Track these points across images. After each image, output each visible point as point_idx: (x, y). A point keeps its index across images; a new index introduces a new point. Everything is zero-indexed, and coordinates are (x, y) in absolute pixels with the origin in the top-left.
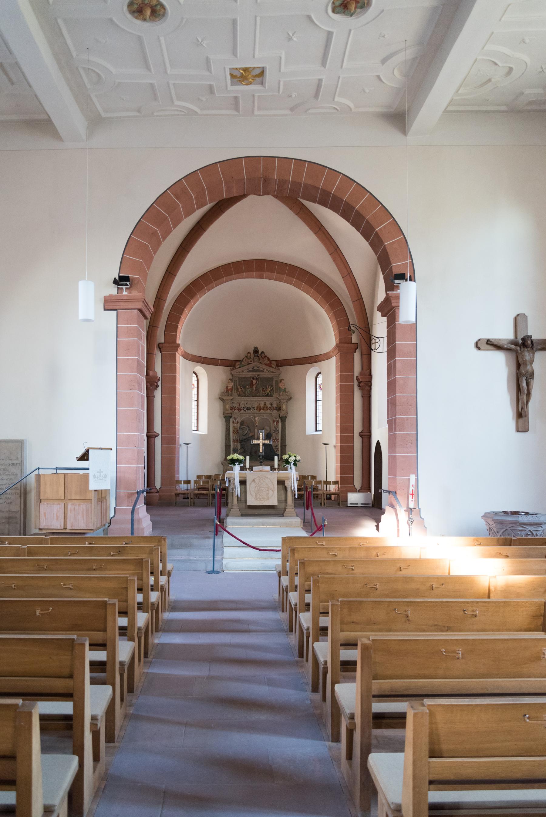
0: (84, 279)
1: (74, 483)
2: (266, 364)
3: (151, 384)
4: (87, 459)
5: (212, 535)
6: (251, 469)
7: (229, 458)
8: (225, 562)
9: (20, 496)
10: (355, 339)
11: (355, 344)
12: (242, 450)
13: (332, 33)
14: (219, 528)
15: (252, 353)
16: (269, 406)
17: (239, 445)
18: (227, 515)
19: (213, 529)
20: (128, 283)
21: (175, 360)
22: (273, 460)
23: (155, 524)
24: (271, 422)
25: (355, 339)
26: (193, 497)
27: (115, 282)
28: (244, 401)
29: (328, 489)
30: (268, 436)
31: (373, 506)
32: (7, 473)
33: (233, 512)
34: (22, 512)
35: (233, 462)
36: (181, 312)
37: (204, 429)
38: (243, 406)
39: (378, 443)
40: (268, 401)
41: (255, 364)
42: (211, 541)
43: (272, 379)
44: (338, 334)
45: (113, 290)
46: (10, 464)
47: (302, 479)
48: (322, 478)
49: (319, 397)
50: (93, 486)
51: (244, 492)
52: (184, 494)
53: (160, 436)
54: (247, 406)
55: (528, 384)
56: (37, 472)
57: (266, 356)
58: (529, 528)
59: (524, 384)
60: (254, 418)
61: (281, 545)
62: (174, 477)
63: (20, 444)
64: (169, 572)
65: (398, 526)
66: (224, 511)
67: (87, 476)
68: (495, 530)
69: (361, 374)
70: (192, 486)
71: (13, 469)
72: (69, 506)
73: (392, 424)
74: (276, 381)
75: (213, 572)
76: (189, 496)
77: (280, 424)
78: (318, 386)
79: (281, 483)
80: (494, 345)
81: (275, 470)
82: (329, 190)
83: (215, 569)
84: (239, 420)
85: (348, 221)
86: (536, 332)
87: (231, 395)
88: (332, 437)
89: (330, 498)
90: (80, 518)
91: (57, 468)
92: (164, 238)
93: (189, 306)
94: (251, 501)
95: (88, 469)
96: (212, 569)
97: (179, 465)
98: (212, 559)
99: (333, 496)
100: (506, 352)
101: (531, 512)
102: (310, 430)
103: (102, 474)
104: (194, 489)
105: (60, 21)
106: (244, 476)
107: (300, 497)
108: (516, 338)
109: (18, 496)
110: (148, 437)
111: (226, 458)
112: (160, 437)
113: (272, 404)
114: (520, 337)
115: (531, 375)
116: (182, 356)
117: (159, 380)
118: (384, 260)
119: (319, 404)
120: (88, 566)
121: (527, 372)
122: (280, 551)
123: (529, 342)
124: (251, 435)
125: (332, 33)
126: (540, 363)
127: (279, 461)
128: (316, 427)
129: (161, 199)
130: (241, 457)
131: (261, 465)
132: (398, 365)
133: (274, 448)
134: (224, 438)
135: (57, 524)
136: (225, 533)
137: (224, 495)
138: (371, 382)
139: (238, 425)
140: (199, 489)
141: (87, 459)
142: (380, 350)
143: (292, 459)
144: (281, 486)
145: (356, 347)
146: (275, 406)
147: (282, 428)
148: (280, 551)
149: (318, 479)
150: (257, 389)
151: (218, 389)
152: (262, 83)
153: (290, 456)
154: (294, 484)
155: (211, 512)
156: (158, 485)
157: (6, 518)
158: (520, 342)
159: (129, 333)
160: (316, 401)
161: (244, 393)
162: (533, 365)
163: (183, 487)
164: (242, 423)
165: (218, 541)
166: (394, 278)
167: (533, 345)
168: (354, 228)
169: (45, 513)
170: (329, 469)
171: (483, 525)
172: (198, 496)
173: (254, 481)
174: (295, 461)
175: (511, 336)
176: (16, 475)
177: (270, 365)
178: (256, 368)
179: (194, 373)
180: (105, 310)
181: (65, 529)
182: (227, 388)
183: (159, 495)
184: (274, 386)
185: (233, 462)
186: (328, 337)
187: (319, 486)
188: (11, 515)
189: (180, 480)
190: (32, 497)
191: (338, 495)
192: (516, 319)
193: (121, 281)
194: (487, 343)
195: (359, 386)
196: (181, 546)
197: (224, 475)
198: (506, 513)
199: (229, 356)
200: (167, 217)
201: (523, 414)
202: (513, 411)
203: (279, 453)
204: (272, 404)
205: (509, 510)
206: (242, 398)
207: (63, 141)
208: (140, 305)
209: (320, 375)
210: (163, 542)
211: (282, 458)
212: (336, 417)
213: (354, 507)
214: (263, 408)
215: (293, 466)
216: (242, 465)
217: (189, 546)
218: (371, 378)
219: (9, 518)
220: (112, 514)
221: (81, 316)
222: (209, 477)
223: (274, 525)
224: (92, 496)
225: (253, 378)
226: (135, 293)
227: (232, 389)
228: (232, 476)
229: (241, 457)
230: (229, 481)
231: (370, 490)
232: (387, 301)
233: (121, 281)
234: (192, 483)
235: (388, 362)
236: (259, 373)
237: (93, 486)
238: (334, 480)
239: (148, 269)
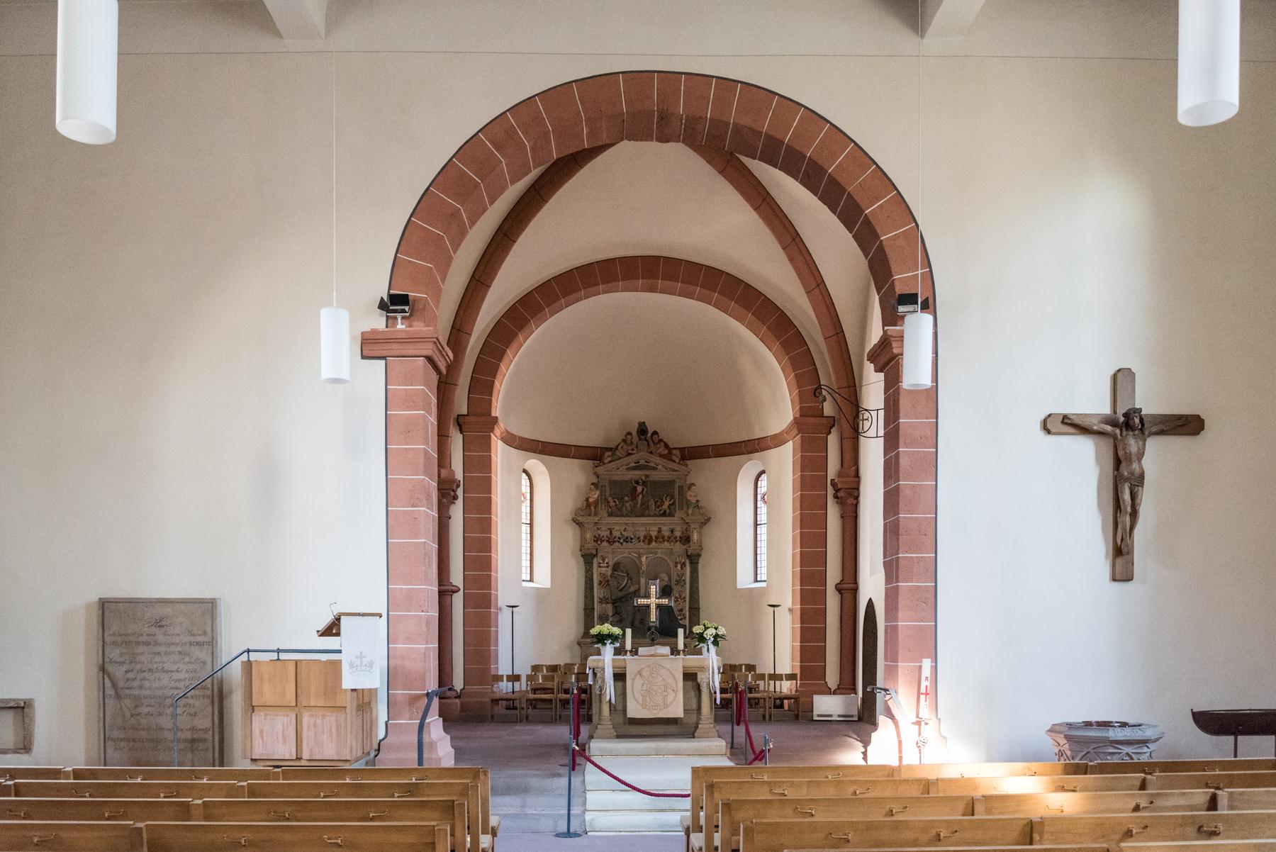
0: (329, 304)
1: (315, 680)
2: (660, 456)
3: (446, 492)
4: (338, 634)
5: (565, 770)
6: (634, 652)
7: (594, 631)
8: (588, 817)
9: (213, 702)
10: (828, 409)
11: (829, 419)
14: (577, 758)
15: (634, 432)
16: (666, 534)
17: (609, 609)
18: (591, 737)
19: (567, 760)
20: (407, 308)
21: (489, 449)
22: (676, 636)
23: (459, 753)
24: (672, 566)
25: (828, 409)
26: (524, 705)
27: (382, 306)
28: (619, 525)
29: (778, 689)
30: (665, 592)
31: (860, 719)
32: (187, 659)
34: (217, 731)
35: (601, 638)
36: (500, 355)
37: (543, 578)
38: (616, 534)
39: (870, 604)
40: (666, 525)
41: (641, 456)
42: (563, 782)
43: (672, 482)
44: (797, 400)
45: (378, 322)
46: (191, 644)
47: (729, 670)
49: (763, 518)
50: (348, 682)
51: (622, 694)
52: (507, 700)
53: (461, 592)
55: (1133, 496)
56: (244, 657)
57: (661, 440)
58: (1126, 749)
59: (1126, 496)
60: (640, 557)
61: (689, 787)
63: (209, 607)
64: (493, 829)
65: (900, 751)
66: (584, 730)
68: (1069, 753)
69: (840, 474)
70: (522, 685)
71: (198, 653)
72: (306, 719)
73: (892, 570)
75: (568, 834)
76: (517, 703)
79: (690, 677)
80: (1074, 425)
81: (678, 653)
82: (780, 137)
83: (572, 830)
84: (611, 560)
85: (816, 194)
86: (1149, 401)
87: (596, 515)
88: (786, 593)
89: (781, 706)
90: (327, 741)
91: (279, 651)
92: (473, 223)
93: (514, 345)
94: (635, 709)
95: (340, 651)
96: (565, 830)
97: (497, 645)
99: (786, 702)
100: (1095, 437)
101: (1131, 722)
102: (744, 579)
103: (364, 662)
104: (527, 691)
107: (726, 704)
108: (1115, 412)
109: (207, 701)
110: (442, 593)
111: (586, 634)
112: (463, 592)
113: (672, 531)
114: (1121, 411)
115: (1139, 480)
116: (502, 439)
117: (458, 486)
118: (880, 268)
119: (762, 530)
120: (359, 810)
121: (1132, 473)
122: (688, 796)
123: (1137, 421)
124: (632, 589)
126: (1156, 457)
127: (685, 637)
129: (467, 150)
131: (652, 645)
132: (904, 462)
133: (677, 613)
134: (582, 595)
135: (285, 751)
136: (589, 765)
137: (583, 701)
138: (858, 489)
139: (609, 571)
140: (535, 691)
141: (338, 634)
142: (872, 433)
143: (709, 633)
144: (690, 683)
145: (832, 423)
146: (678, 534)
147: (692, 577)
148: (688, 796)
150: (644, 498)
151: (570, 504)
153: (706, 628)
155: (562, 732)
156: (458, 683)
157: (185, 741)
158: (1122, 419)
160: (756, 525)
161: (620, 510)
162: (1143, 462)
163: (505, 687)
164: (616, 567)
166: (898, 302)
167: (1143, 425)
168: (825, 207)
169: (261, 732)
170: (780, 652)
171: (1049, 745)
172: (533, 703)
173: (640, 673)
174: (716, 636)
175: (1106, 410)
176: (204, 663)
177: (668, 456)
178: (642, 462)
179: (525, 471)
180: (363, 357)
181: (298, 759)
182: (587, 500)
183: (462, 704)
184: (677, 496)
185: (601, 638)
186: (778, 406)
187: (761, 683)
188: (195, 736)
189: (500, 673)
190: (236, 703)
191: (796, 699)
192: (1115, 377)
193: (393, 304)
194: (1063, 422)
195: (836, 497)
196: (508, 791)
197: (583, 665)
198: (1088, 724)
199: (590, 437)
201: (1124, 550)
202: (1107, 545)
203: (687, 622)
204: (672, 531)
205: (1094, 719)
206: (616, 520)
207: (276, 33)
208: (428, 349)
209: (764, 477)
210: (482, 776)
211: (691, 632)
212: (794, 555)
213: (826, 722)
215: (711, 646)
216: (618, 645)
217: (525, 790)
218: (858, 483)
219: (193, 740)
220: (381, 734)
221: (326, 373)
222: (554, 668)
223: (677, 753)
224: (348, 701)
225: (637, 482)
226: (419, 327)
228: (600, 665)
230: (595, 674)
231: (854, 691)
232: (885, 342)
233: (395, 303)
234: (524, 679)
235: (886, 453)
236: (647, 472)
237: (348, 682)
238: (789, 672)
239: (443, 280)
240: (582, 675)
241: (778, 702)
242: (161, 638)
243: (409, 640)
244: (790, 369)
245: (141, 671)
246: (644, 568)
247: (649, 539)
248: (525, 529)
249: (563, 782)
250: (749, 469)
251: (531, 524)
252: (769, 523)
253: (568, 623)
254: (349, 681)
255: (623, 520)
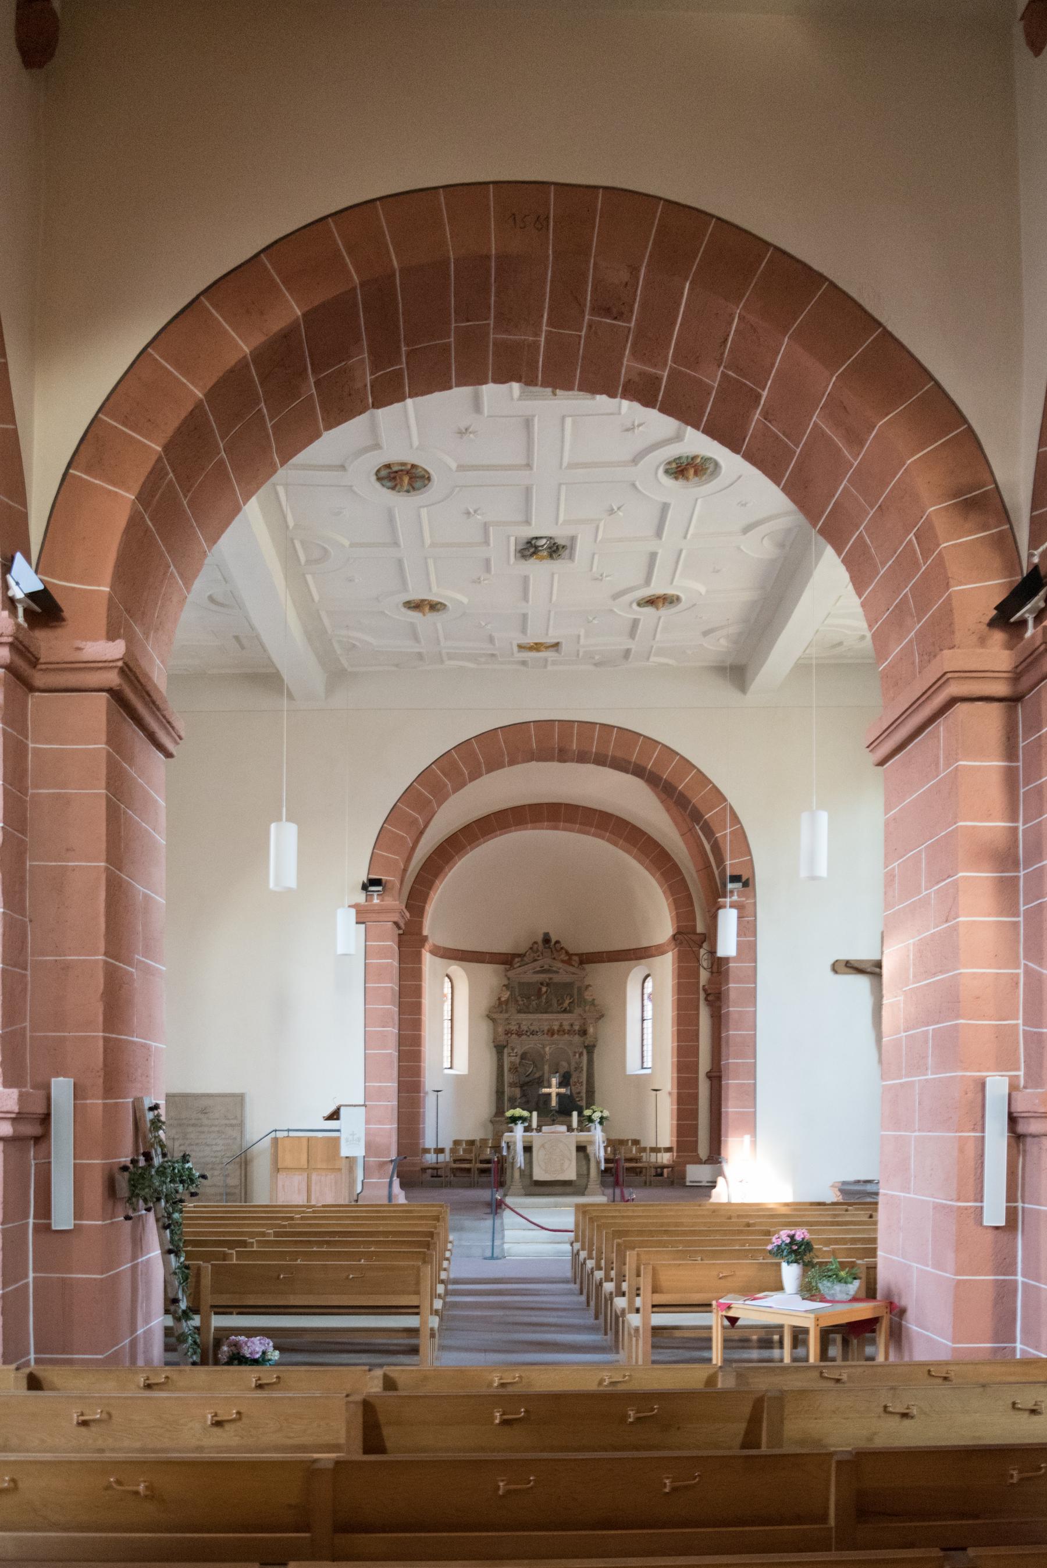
1: (324, 1150)
2: (563, 961)
6: (539, 1130)
7: (509, 1113)
8: (506, 1246)
11: (694, 940)
12: (524, 1100)
13: (639, 620)
14: (496, 1207)
16: (567, 1027)
17: (517, 1092)
22: (570, 1115)
27: (365, 887)
28: (527, 1020)
29: (659, 1160)
30: (564, 1082)
33: (513, 1189)
35: (514, 1120)
37: (462, 1067)
38: (524, 1028)
40: (566, 1019)
41: (545, 962)
45: (361, 898)
48: (649, 1142)
49: (648, 1014)
51: (529, 1162)
54: (532, 1028)
56: (273, 1135)
57: (562, 948)
60: (544, 1048)
62: (418, 1144)
63: (239, 1099)
67: (338, 1139)
72: (314, 1177)
74: (579, 989)
75: (492, 1258)
77: (585, 1057)
78: (646, 996)
79: (581, 1149)
84: (519, 1050)
87: (507, 1012)
88: (666, 1081)
89: (661, 1175)
90: (327, 1192)
91: (288, 1130)
94: (539, 1175)
97: (424, 1123)
98: (490, 1244)
99: (665, 1170)
102: (633, 1067)
105: (323, 614)
106: (529, 1139)
107: (607, 1170)
109: (237, 1166)
113: (572, 1025)
119: (648, 1024)
124: (537, 1075)
125: (639, 620)
128: (643, 1063)
130: (525, 1114)
134: (494, 1077)
135: (300, 1199)
139: (518, 1060)
140: (455, 1161)
141: (338, 1119)
143: (596, 1116)
144: (581, 1154)
146: (577, 1028)
149: (643, 1145)
150: (549, 996)
151: (485, 1002)
152: (557, 651)
154: (599, 1151)
155: (485, 1194)
159: (382, 953)
161: (528, 1007)
163: (430, 1158)
164: (524, 1056)
165: (498, 1222)
170: (661, 1130)
172: (454, 1171)
173: (543, 1146)
174: (602, 1118)
176: (235, 1139)
177: (569, 962)
178: (546, 967)
182: (499, 999)
184: (576, 996)
185: (514, 1120)
186: (661, 924)
195: (706, 999)
198: (858, 1182)
199: (503, 947)
200: (430, 801)
206: (522, 1016)
208: (396, 918)
209: (649, 979)
214: (558, 1031)
220: (359, 1190)
221: (340, 951)
222: (472, 1143)
224: (343, 1165)
225: (542, 984)
227: (507, 1002)
229: (525, 1114)
230: (508, 1147)
234: (447, 1151)
236: (551, 976)
238: (667, 1145)
240: (497, 1148)
241: (659, 1170)
242: (206, 1122)
243: (380, 1122)
244: (669, 893)
245: (190, 1145)
246: (547, 1057)
247: (551, 1032)
248: (447, 1024)
249: (489, 1223)
250: (637, 971)
251: (452, 1020)
252: (654, 1018)
253: (483, 1104)
254: (345, 1151)
255: (531, 1016)
